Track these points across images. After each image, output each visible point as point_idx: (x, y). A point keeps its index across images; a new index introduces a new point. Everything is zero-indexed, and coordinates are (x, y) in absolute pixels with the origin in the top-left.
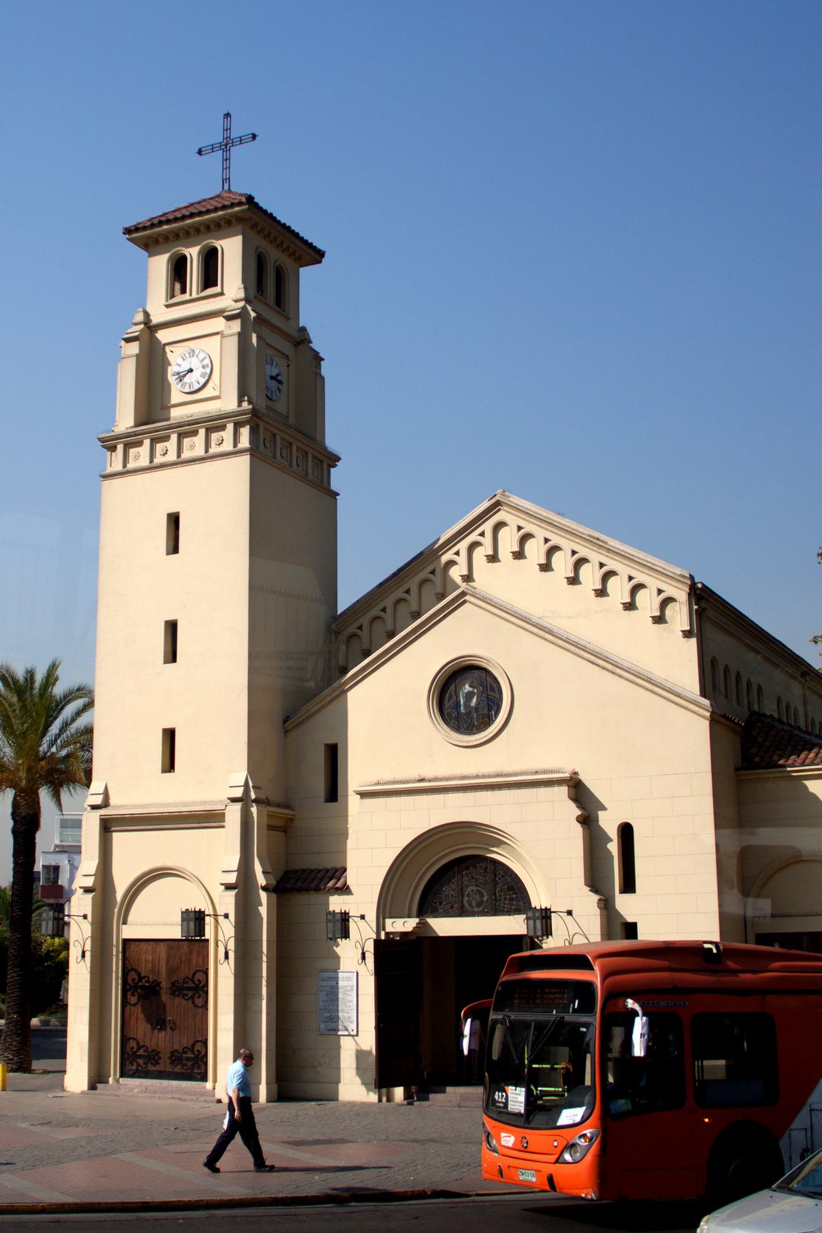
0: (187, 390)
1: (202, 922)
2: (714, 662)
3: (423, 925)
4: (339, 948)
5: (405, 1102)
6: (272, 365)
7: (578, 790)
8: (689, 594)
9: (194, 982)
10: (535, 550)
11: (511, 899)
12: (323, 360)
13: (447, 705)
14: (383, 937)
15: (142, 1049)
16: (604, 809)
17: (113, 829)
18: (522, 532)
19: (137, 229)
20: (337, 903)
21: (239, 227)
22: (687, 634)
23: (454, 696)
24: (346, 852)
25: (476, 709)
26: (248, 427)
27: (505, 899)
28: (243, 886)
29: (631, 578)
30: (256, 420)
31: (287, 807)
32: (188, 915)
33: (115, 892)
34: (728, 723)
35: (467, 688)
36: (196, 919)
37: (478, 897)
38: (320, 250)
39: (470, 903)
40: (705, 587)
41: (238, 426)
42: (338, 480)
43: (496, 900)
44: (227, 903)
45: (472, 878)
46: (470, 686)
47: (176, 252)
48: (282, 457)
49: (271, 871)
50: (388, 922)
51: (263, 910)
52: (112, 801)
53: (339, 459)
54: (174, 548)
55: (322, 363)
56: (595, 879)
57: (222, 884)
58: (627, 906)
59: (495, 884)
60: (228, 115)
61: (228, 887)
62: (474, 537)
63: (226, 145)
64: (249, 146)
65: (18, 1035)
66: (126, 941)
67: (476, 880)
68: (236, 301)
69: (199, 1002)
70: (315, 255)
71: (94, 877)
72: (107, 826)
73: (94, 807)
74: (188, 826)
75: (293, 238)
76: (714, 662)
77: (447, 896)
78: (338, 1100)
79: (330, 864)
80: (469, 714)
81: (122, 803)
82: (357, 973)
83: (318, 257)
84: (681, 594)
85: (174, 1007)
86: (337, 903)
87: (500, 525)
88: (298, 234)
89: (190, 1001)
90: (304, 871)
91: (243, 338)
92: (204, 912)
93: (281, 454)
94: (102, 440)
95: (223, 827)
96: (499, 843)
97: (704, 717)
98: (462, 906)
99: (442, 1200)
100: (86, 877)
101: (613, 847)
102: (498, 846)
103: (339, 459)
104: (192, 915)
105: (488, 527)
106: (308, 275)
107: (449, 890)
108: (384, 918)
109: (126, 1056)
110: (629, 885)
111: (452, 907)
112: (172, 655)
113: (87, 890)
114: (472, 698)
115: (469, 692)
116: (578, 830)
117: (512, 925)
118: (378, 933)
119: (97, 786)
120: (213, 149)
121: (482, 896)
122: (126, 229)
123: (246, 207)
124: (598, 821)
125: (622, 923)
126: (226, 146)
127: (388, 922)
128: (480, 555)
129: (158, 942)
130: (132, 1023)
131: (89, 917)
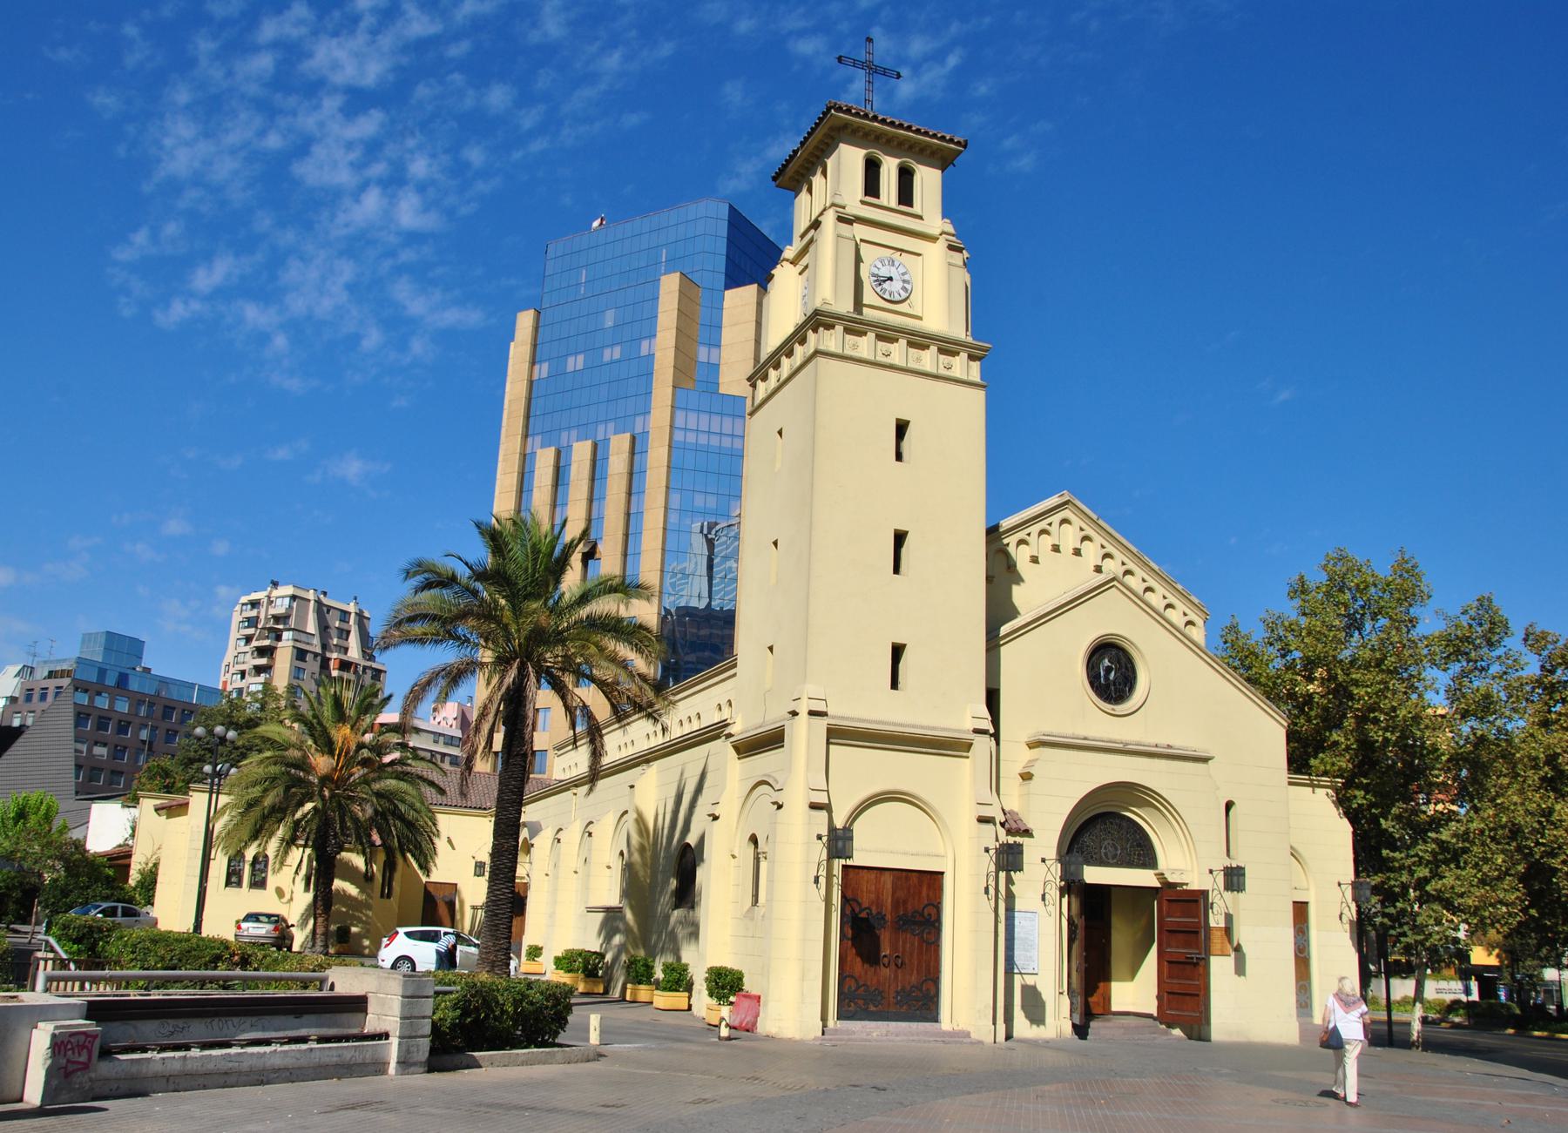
4: (1014, 887)
9: (923, 916)
15: (862, 989)
25: (1114, 682)
27: (1135, 854)
35: (1106, 662)
39: (1106, 854)
46: (1109, 661)
47: (905, 162)
67: (1112, 834)
74: (924, 750)
77: (1088, 846)
78: (1210, 1041)
97: (1282, 725)
100: (981, 806)
102: (1139, 807)
114: (1111, 672)
121: (1116, 849)
129: (883, 872)
130: (849, 959)
131: (825, 839)
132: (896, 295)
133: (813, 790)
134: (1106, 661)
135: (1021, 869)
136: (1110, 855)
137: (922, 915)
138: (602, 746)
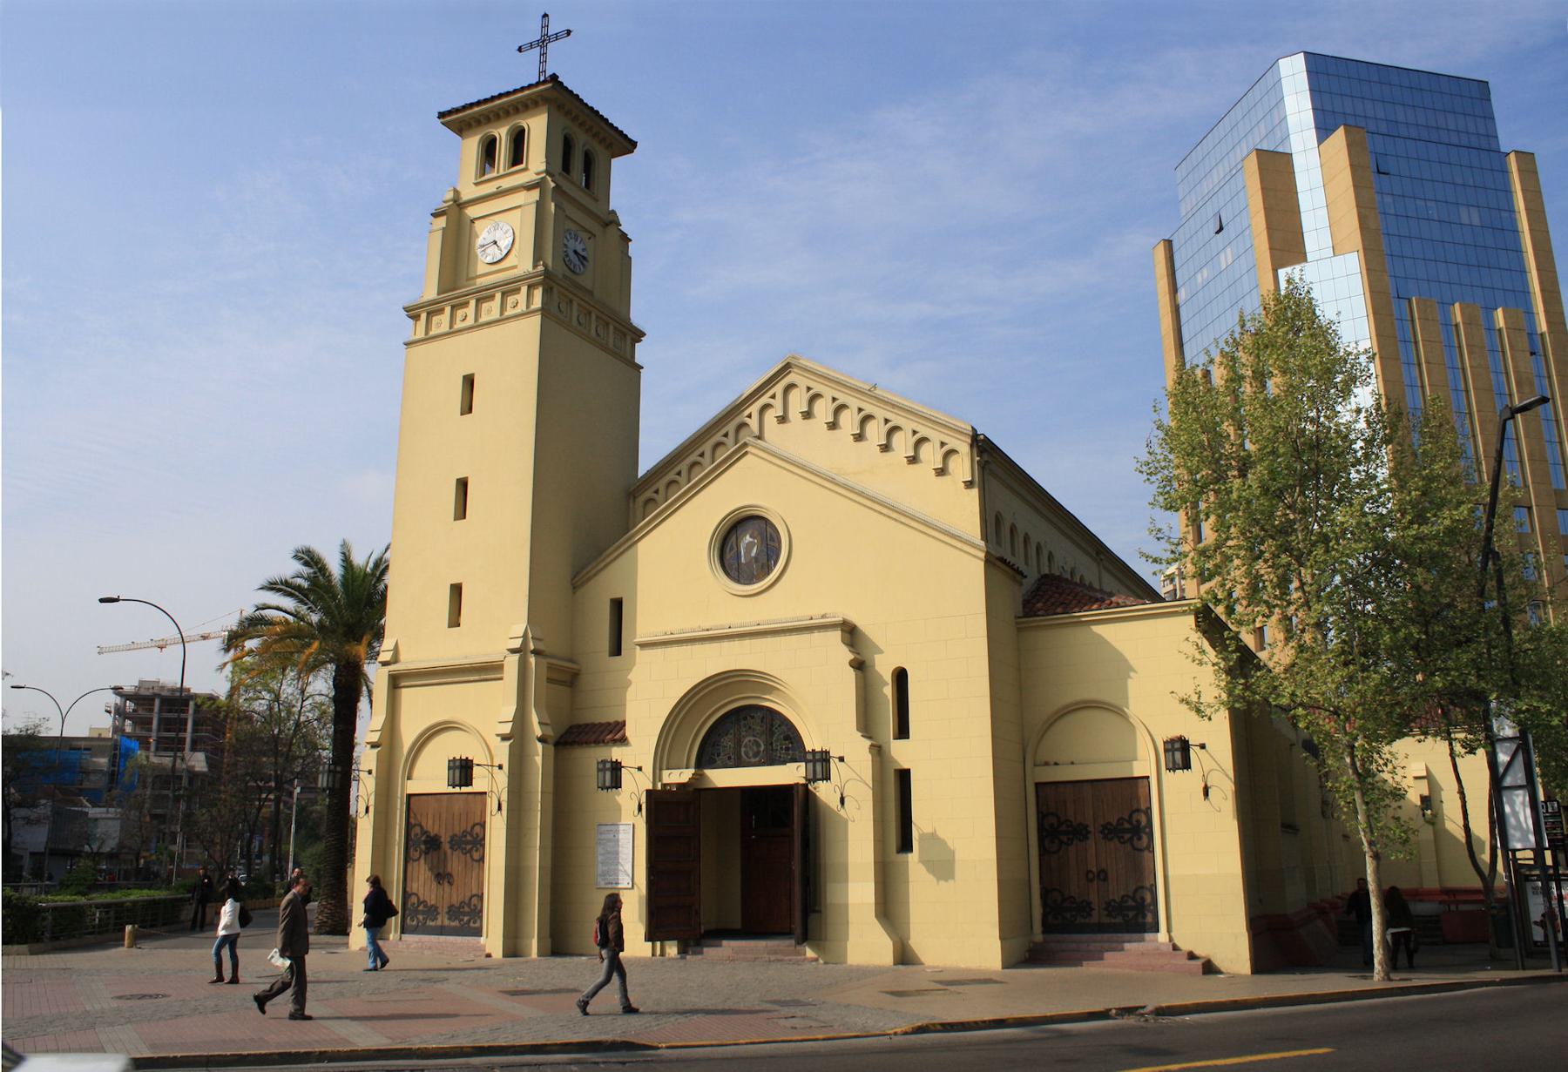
1: (469, 770)
2: (998, 520)
3: (699, 776)
5: (679, 956)
6: (577, 240)
7: (850, 633)
8: (971, 446)
10: (823, 410)
11: (787, 749)
12: (631, 240)
13: (728, 556)
14: (659, 787)
16: (881, 652)
17: (403, 684)
18: (811, 392)
19: (450, 113)
20: (617, 753)
21: (545, 108)
22: (969, 485)
23: (735, 546)
24: (625, 705)
25: (756, 559)
26: (541, 289)
27: (781, 748)
28: (517, 737)
29: (915, 432)
30: (548, 281)
31: (571, 661)
32: (454, 763)
33: (402, 748)
34: (1007, 569)
35: (748, 539)
36: (461, 767)
37: (755, 748)
38: (630, 140)
40: (987, 440)
41: (530, 287)
42: (642, 353)
43: (772, 750)
44: (502, 752)
45: (750, 728)
46: (751, 537)
48: (560, 311)
49: (548, 722)
50: (665, 773)
51: (539, 760)
52: (402, 657)
53: (643, 334)
54: (467, 408)
55: (630, 243)
56: (866, 724)
57: (498, 735)
58: (902, 753)
59: (772, 734)
61: (504, 738)
62: (765, 400)
63: (543, 42)
65: (334, 898)
66: (410, 796)
68: (538, 174)
69: (476, 856)
70: (628, 146)
71: (379, 733)
72: (395, 682)
73: (385, 664)
75: (603, 124)
76: (998, 520)
79: (612, 718)
80: (748, 564)
81: (408, 662)
82: (634, 825)
83: (630, 147)
84: (964, 447)
85: (455, 863)
86: (617, 753)
87: (790, 387)
88: (607, 120)
89: (468, 855)
90: (587, 725)
91: (540, 206)
92: (472, 761)
93: (578, 320)
94: (407, 309)
95: (501, 679)
96: (771, 689)
98: (739, 757)
101: (888, 691)
102: (770, 693)
103: (643, 334)
104: (458, 763)
105: (778, 389)
106: (619, 165)
107: (727, 742)
108: (661, 769)
109: (407, 912)
110: (903, 731)
112: (461, 512)
113: (374, 746)
115: (750, 542)
116: (851, 674)
117: (789, 774)
118: (654, 784)
119: (388, 644)
120: (531, 46)
121: (758, 745)
122: (439, 113)
123: (550, 85)
124: (874, 666)
125: (895, 770)
126: (543, 42)
127: (665, 773)
128: (770, 416)
134: (748, 537)
135: (647, 791)
136: (751, 754)
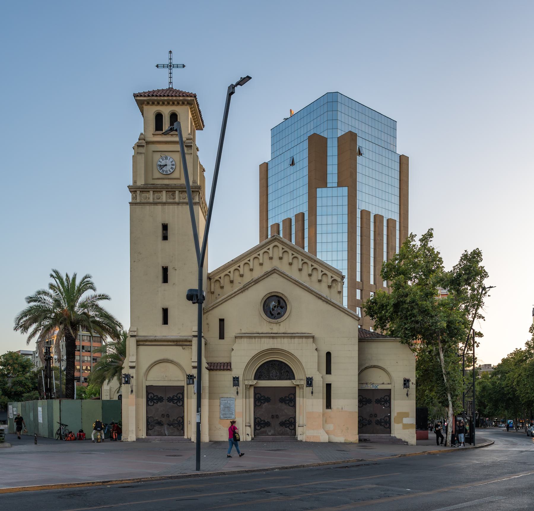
0: (165, 173)
60: (170, 52)
64: (174, 55)
99: (128, 479)
111: (266, 377)
132: (168, 171)
133: (131, 362)
137: (154, 402)
138: (52, 444)
